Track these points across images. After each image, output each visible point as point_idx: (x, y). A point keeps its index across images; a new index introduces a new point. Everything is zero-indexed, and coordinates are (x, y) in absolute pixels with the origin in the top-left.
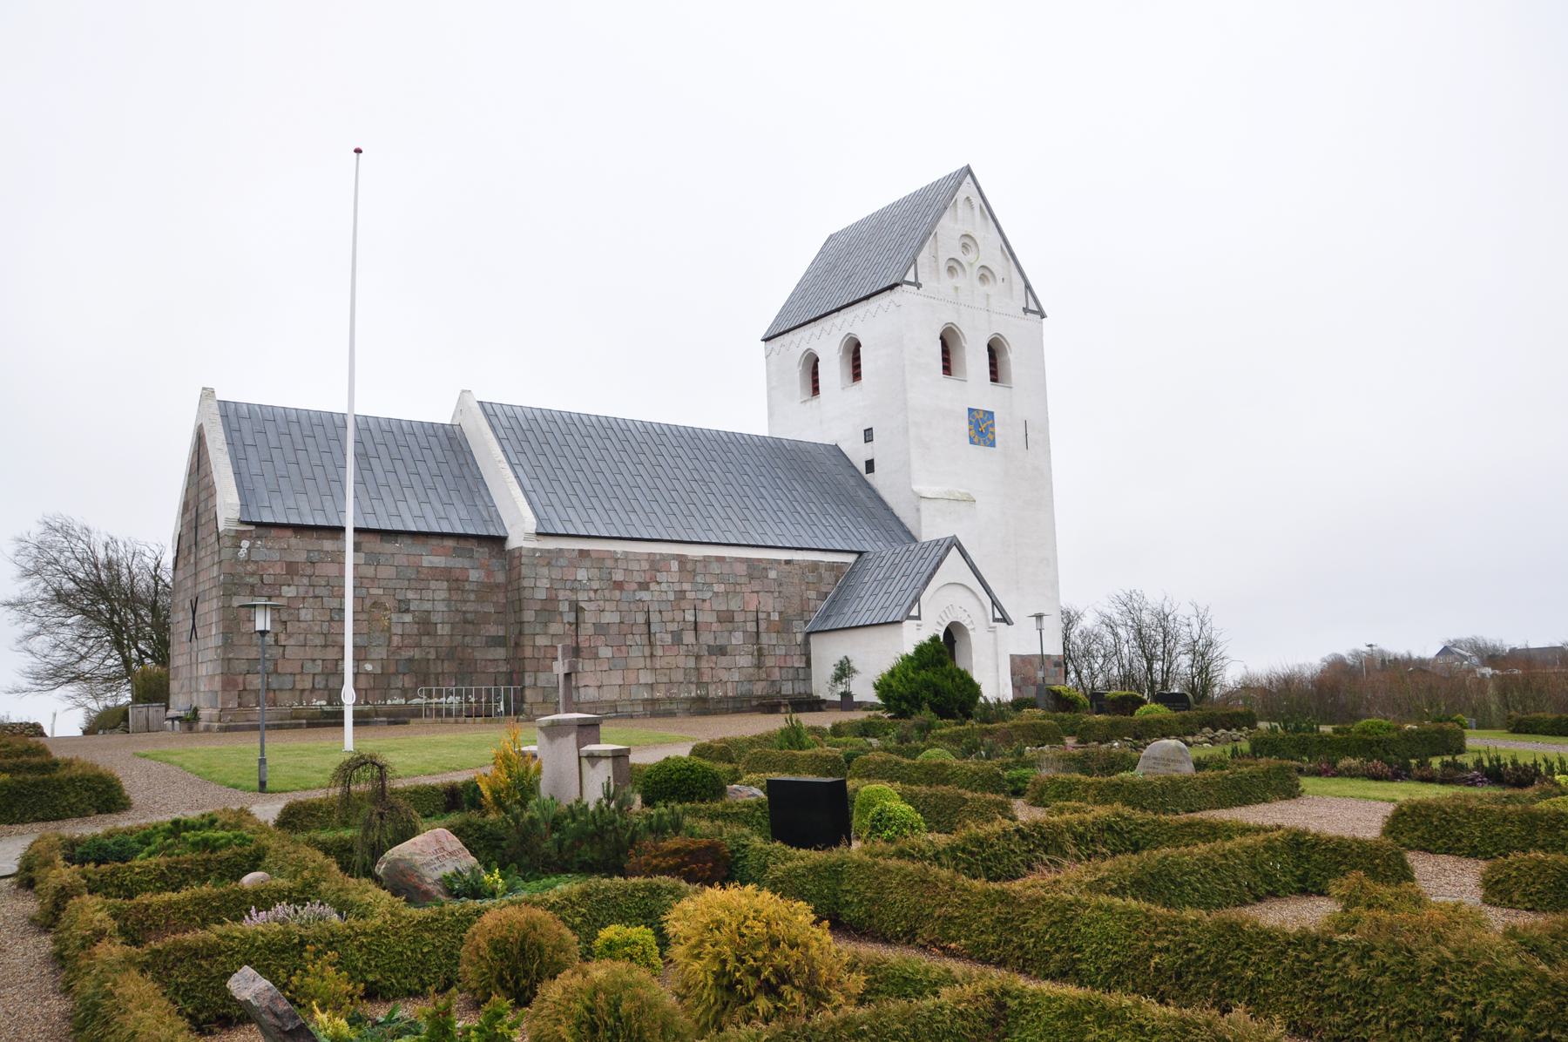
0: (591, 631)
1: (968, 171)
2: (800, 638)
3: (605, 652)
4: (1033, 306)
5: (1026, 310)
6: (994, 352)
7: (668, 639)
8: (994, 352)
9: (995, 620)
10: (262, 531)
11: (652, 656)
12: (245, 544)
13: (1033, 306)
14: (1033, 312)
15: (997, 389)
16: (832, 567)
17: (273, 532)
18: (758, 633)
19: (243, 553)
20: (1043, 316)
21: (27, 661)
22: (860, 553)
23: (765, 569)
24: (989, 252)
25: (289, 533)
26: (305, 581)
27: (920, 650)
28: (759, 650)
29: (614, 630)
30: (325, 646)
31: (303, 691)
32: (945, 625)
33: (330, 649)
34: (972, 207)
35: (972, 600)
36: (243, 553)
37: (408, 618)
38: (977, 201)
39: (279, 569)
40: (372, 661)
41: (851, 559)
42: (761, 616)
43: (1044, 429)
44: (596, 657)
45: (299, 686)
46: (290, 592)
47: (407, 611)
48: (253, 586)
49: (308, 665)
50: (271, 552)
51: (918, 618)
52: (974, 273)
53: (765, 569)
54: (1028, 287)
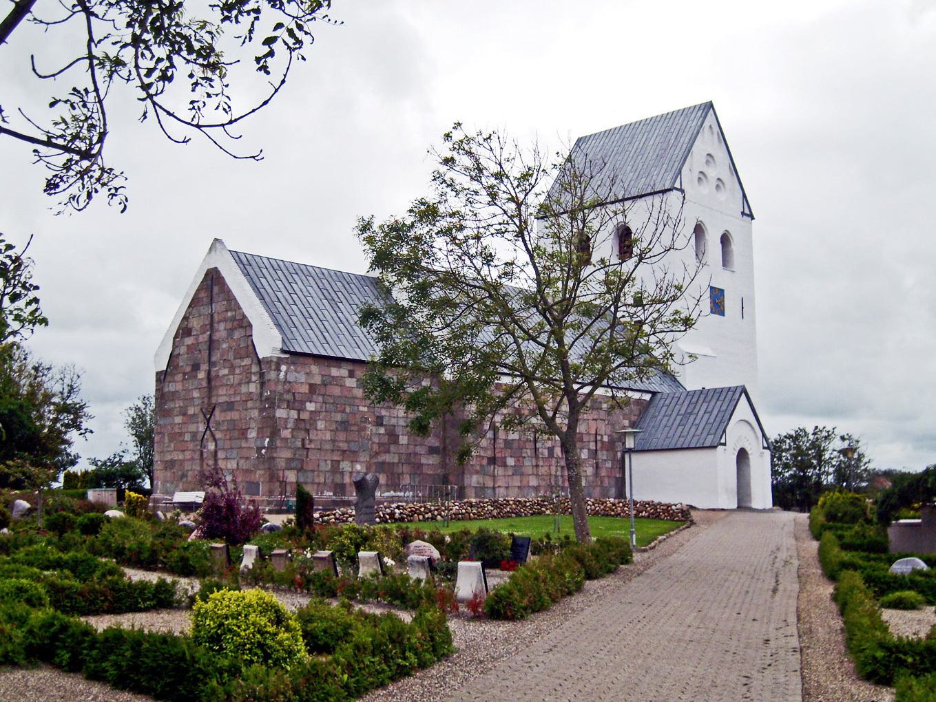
0: (502, 445)
1: (710, 106)
2: (619, 455)
3: (511, 462)
4: (747, 211)
5: (743, 213)
6: (725, 240)
7: (546, 452)
8: (725, 240)
9: (764, 448)
10: (294, 359)
11: (537, 466)
12: (284, 368)
13: (747, 211)
14: (747, 215)
15: (726, 274)
16: (638, 402)
17: (301, 359)
18: (596, 450)
19: (282, 374)
20: (753, 218)
21: (860, 451)
22: (654, 394)
23: (600, 403)
24: (720, 170)
25: (310, 360)
26: (320, 399)
27: (308, 494)
28: (597, 464)
29: (515, 445)
30: (333, 451)
31: (319, 484)
32: (738, 449)
33: (335, 453)
34: (712, 133)
35: (751, 432)
36: (282, 374)
37: (382, 430)
38: (716, 129)
39: (305, 389)
40: (361, 462)
41: (647, 397)
42: (599, 438)
43: (752, 300)
44: (505, 465)
45: (317, 481)
46: (310, 406)
47: (382, 425)
48: (288, 401)
49: (322, 464)
50: (300, 378)
51: (724, 444)
52: (714, 183)
53: (600, 403)
54: (744, 196)
